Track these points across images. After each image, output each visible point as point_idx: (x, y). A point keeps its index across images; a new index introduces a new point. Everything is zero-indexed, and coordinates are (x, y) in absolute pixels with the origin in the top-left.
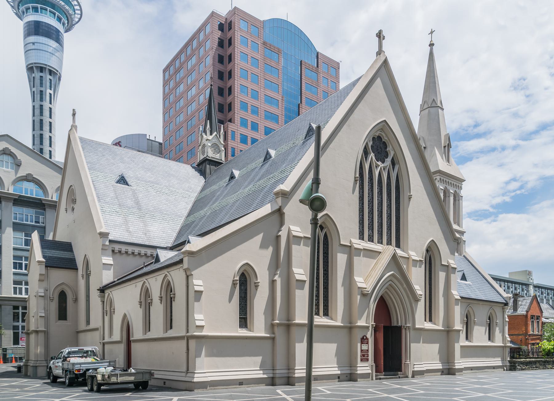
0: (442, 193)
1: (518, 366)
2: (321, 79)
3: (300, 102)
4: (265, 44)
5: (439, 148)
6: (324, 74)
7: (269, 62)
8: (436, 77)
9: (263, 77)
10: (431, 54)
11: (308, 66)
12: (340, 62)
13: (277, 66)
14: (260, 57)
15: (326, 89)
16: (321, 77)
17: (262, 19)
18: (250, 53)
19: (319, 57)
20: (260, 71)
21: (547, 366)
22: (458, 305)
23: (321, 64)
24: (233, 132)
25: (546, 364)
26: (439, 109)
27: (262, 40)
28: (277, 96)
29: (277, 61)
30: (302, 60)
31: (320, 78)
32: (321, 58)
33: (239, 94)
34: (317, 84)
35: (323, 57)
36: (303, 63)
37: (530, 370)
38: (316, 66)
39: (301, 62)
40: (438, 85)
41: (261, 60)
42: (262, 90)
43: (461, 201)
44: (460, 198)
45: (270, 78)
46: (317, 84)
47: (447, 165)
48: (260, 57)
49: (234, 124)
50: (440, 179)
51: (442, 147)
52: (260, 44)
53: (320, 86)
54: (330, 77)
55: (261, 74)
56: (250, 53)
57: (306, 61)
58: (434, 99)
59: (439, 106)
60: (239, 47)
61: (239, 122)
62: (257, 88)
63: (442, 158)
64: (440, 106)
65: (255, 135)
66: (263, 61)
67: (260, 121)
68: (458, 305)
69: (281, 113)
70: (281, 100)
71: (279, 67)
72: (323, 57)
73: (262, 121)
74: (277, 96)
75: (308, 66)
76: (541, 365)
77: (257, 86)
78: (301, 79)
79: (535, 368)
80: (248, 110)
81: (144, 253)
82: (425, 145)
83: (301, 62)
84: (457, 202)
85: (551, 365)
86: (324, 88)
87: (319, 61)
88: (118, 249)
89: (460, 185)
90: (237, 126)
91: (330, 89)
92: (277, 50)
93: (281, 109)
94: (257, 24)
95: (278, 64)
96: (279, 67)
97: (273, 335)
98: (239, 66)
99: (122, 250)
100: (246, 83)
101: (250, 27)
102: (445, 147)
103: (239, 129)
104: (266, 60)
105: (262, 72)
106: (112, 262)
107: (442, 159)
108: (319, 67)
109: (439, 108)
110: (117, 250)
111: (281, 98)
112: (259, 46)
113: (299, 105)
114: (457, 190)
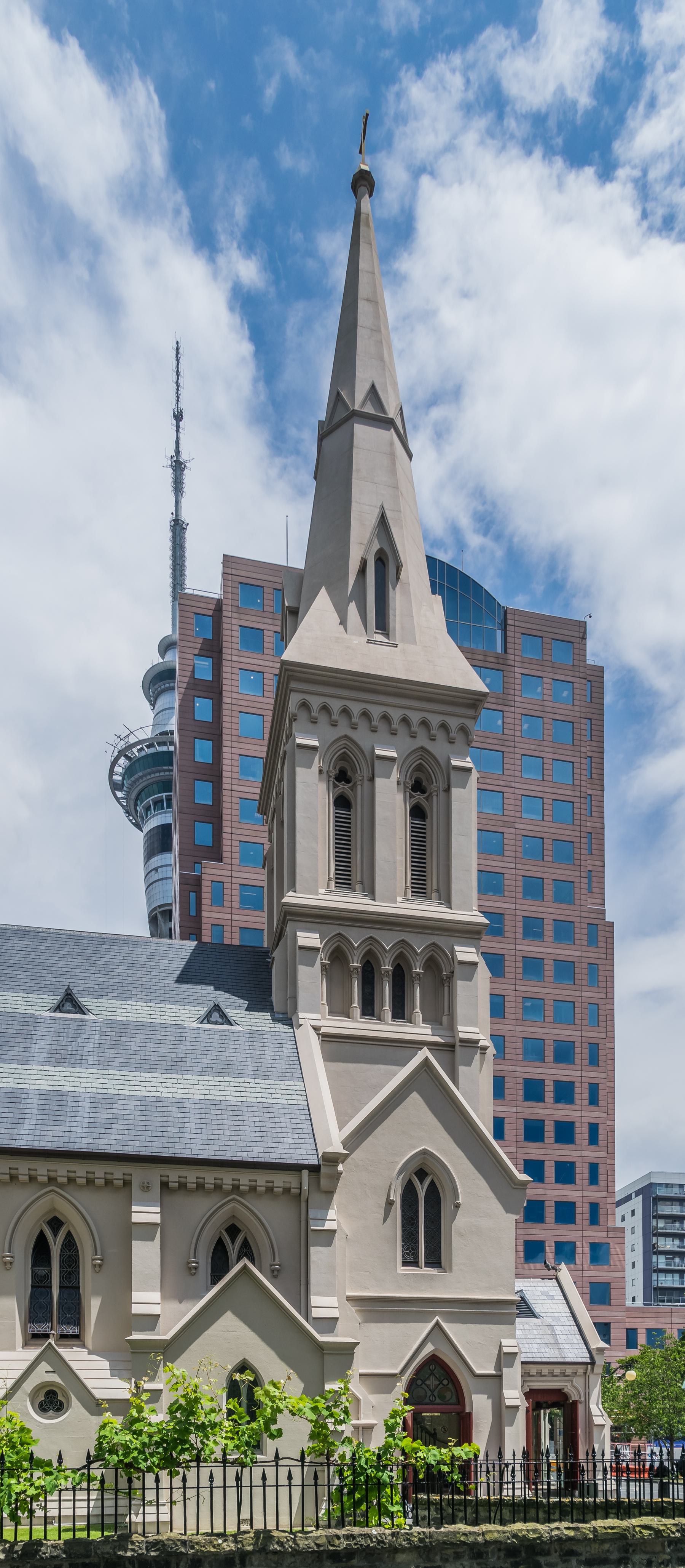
2: (517, 681)
15: (536, 708)
16: (518, 676)
24: (218, 885)
32: (517, 623)
33: (234, 782)
34: (501, 701)
49: (221, 862)
53: (512, 703)
60: (234, 658)
61: (237, 855)
68: (152, 1239)
81: (213, 1182)
86: (526, 706)
88: (264, 1184)
90: (229, 867)
97: (499, 1373)
98: (234, 708)
99: (275, 1185)
102: (362, 571)
103: (234, 874)
106: (156, 1218)
110: (176, 1182)
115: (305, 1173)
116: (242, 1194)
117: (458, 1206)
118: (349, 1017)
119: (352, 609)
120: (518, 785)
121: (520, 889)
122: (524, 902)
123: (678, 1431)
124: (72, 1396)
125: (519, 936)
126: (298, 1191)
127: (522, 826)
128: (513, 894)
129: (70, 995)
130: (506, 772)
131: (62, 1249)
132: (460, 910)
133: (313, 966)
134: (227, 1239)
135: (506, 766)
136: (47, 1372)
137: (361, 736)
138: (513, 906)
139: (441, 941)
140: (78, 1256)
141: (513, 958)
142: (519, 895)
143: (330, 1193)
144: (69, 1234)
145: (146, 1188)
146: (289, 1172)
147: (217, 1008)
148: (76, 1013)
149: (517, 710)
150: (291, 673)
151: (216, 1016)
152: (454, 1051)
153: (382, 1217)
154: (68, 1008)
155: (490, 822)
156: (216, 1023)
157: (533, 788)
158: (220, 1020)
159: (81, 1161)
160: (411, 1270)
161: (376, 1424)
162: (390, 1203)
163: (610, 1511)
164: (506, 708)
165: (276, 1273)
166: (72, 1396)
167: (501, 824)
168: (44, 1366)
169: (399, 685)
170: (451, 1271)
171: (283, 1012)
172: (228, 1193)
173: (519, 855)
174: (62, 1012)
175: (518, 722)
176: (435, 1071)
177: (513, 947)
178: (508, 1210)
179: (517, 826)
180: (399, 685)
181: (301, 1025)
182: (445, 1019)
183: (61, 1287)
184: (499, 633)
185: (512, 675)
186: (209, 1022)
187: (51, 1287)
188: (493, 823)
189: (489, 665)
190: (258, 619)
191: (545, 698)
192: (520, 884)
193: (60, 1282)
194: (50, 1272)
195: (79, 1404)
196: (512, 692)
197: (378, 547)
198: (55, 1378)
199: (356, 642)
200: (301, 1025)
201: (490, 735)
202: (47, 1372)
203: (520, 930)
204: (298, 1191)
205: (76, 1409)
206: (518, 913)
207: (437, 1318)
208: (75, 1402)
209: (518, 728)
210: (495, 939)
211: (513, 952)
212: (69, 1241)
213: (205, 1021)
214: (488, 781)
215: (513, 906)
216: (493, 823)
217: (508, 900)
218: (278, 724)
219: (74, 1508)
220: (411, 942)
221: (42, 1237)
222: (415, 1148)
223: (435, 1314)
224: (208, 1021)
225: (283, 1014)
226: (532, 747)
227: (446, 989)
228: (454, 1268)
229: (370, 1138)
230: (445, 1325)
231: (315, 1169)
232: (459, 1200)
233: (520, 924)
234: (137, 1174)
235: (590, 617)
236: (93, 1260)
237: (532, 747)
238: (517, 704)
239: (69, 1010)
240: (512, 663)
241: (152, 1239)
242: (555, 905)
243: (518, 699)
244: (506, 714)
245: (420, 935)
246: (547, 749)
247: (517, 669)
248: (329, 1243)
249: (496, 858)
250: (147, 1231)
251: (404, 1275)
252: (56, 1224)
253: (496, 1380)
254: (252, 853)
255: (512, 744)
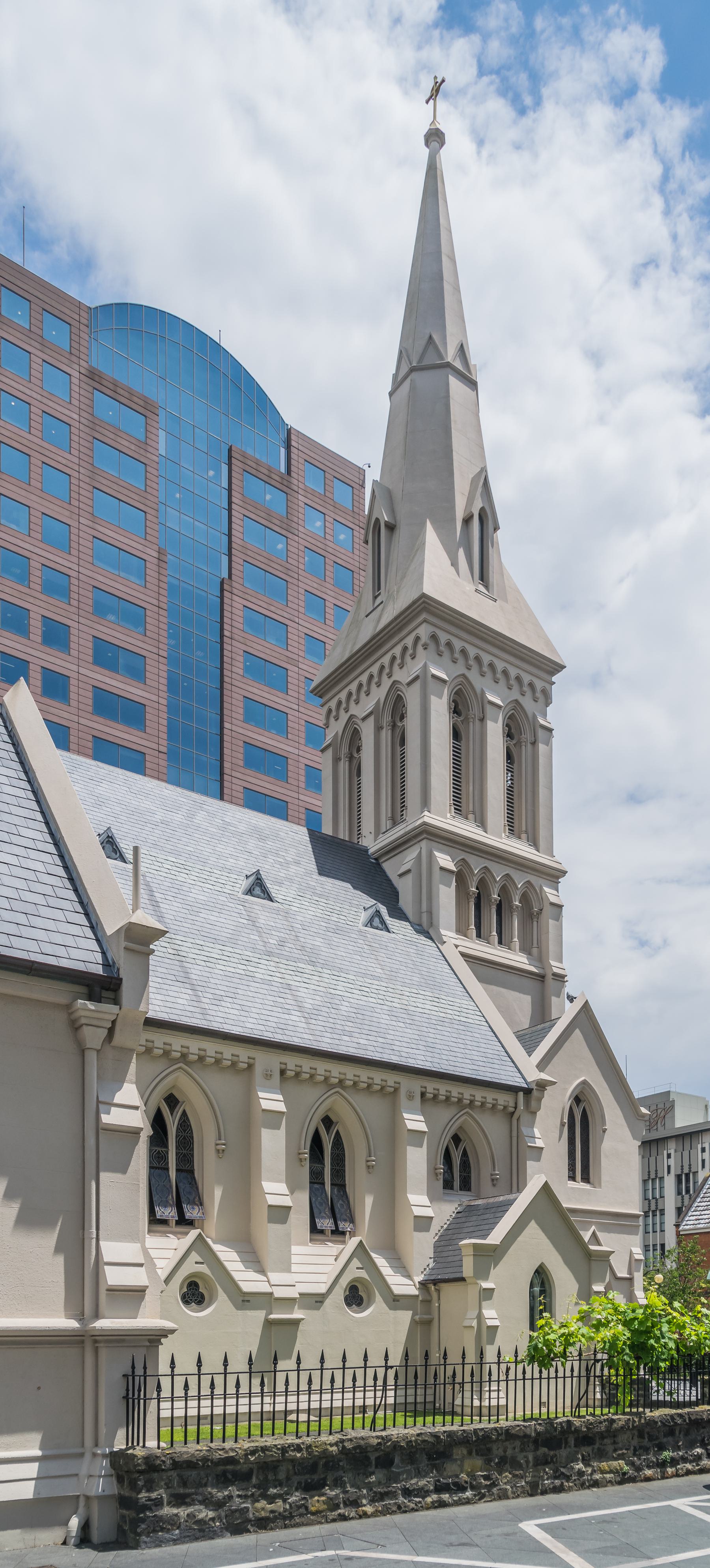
0: (440, 697)
1: (180, 1500)
2: (301, 510)
3: (225, 575)
4: (97, 378)
5: (444, 526)
6: (309, 496)
7: (112, 436)
8: (444, 259)
9: (87, 480)
10: (433, 173)
11: (254, 465)
12: (366, 468)
13: (142, 452)
14: (76, 417)
15: (319, 544)
17: (93, 306)
18: (39, 398)
19: (293, 443)
20: (76, 460)
21: (580, 1466)
22: (421, 1146)
23: (301, 466)
25: (563, 1453)
26: (450, 377)
27: (82, 363)
28: (140, 547)
29: (143, 440)
30: (231, 446)
31: (296, 507)
32: (301, 448)
34: (284, 526)
35: (306, 444)
36: (234, 454)
37: (365, 1515)
38: (283, 469)
39: (230, 450)
40: (457, 289)
41: (82, 427)
42: (82, 520)
43: (542, 747)
44: (541, 733)
45: (116, 487)
46: (284, 526)
47: (476, 590)
48: (76, 417)
50: (434, 637)
51: (454, 519)
52: (77, 374)
54: (331, 508)
55: (82, 470)
56: (39, 398)
57: (250, 451)
58: (431, 337)
59: (448, 365)
62: (67, 513)
63: (454, 564)
64: (458, 364)
65: (58, 662)
66: (87, 430)
67: (76, 618)
68: (421, 1146)
69: (155, 602)
70: (156, 561)
71: (149, 455)
72: (306, 444)
73: (82, 620)
74: (140, 547)
75: (254, 465)
76: (505, 1463)
77: (66, 506)
78: (230, 503)
79: (435, 1497)
80: (32, 578)
82: (392, 511)
83: (230, 450)
84: (526, 751)
85: (621, 1457)
87: (293, 456)
89: (539, 685)
91: (331, 544)
92: (142, 403)
93: (156, 589)
94: (68, 312)
95: (142, 446)
96: (149, 455)
99: (499, 1103)
100: (23, 493)
101: (39, 317)
102: (467, 521)
104: (98, 428)
105: (82, 463)
106: (281, 1107)
107: (452, 565)
108: (293, 474)
109: (449, 370)
110: (195, 1054)
111: (155, 554)
112: (75, 381)
113: (222, 583)
114: (527, 703)
115: (521, 1094)
116: (189, 1063)
117: (604, 1131)
118: (465, 936)
119: (461, 553)
120: (301, 622)
121: (303, 735)
122: (306, 749)
123: (660, 1329)
124: (376, 1291)
125: (302, 785)
126: (513, 1109)
127: (304, 667)
128: (296, 739)
129: (260, 879)
130: (290, 604)
131: (178, 1129)
132: (493, 836)
133: (450, 887)
134: (452, 1148)
135: (290, 598)
136: (358, 1268)
137: (473, 676)
138: (296, 751)
139: (535, 880)
140: (192, 1138)
141: (296, 808)
142: (302, 741)
143: (534, 1113)
144: (184, 1113)
145: (268, 1076)
146: (403, 1074)
147: (378, 913)
148: (264, 899)
149: (301, 541)
150: (427, 606)
151: (257, 890)
152: (543, 981)
153: (557, 1136)
154: (258, 893)
155: (274, 654)
156: (377, 928)
157: (315, 629)
158: (380, 926)
159: (364, 1066)
160: (571, 1184)
161: (303, 1319)
162: (562, 1125)
163: (654, 1398)
164: (290, 535)
165: (495, 1182)
166: (376, 1291)
167: (285, 659)
168: (194, 1256)
169: (505, 641)
170: (600, 1186)
171: (418, 923)
172: (176, 1061)
173: (302, 697)
174: (252, 896)
175: (301, 554)
176: (591, 1013)
177: (296, 795)
178: (634, 1138)
179: (301, 666)
180: (505, 641)
181: (445, 942)
182: (535, 951)
183: (178, 1170)
184: (283, 451)
185: (296, 501)
186: (372, 927)
187: (167, 1169)
188: (277, 655)
189: (273, 483)
190: (23, 338)
191: (328, 537)
192: (303, 729)
193: (177, 1165)
194: (323, 1169)
195: (381, 1299)
196: (295, 519)
197: (481, 505)
198: (204, 1269)
199: (468, 588)
200: (445, 942)
201: (274, 559)
202: (358, 1268)
203: (302, 779)
204: (513, 1109)
205: (221, 1305)
206: (301, 759)
207: (593, 1228)
208: (378, 1298)
209: (301, 560)
210: (279, 783)
211: (296, 802)
212: (184, 1121)
213: (369, 925)
214: (272, 608)
215: (296, 751)
216: (277, 655)
217: (291, 743)
218: (387, 636)
219: (212, 1406)
220: (492, 871)
221: (447, 1150)
222: (578, 1078)
223: (591, 1223)
224: (371, 924)
225: (418, 925)
226: (315, 585)
227: (535, 923)
228: (603, 1184)
229: (550, 1066)
230: (598, 1234)
231: (528, 1092)
232: (606, 1125)
233: (302, 772)
234: (265, 1060)
235: (369, 467)
236: (217, 1145)
237: (315, 585)
238: (301, 535)
239: (258, 894)
240: (296, 488)
241: (278, 1128)
242: (42, 648)
243: (301, 529)
244: (290, 541)
245: (518, 872)
246: (329, 592)
247: (300, 497)
248: (538, 1159)
249: (279, 694)
250: (273, 1119)
251: (572, 1188)
252: (328, 1122)
253: (626, 1283)
254: (110, 654)
255: (296, 576)
